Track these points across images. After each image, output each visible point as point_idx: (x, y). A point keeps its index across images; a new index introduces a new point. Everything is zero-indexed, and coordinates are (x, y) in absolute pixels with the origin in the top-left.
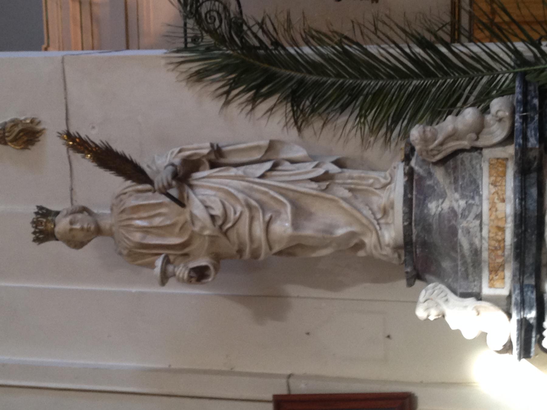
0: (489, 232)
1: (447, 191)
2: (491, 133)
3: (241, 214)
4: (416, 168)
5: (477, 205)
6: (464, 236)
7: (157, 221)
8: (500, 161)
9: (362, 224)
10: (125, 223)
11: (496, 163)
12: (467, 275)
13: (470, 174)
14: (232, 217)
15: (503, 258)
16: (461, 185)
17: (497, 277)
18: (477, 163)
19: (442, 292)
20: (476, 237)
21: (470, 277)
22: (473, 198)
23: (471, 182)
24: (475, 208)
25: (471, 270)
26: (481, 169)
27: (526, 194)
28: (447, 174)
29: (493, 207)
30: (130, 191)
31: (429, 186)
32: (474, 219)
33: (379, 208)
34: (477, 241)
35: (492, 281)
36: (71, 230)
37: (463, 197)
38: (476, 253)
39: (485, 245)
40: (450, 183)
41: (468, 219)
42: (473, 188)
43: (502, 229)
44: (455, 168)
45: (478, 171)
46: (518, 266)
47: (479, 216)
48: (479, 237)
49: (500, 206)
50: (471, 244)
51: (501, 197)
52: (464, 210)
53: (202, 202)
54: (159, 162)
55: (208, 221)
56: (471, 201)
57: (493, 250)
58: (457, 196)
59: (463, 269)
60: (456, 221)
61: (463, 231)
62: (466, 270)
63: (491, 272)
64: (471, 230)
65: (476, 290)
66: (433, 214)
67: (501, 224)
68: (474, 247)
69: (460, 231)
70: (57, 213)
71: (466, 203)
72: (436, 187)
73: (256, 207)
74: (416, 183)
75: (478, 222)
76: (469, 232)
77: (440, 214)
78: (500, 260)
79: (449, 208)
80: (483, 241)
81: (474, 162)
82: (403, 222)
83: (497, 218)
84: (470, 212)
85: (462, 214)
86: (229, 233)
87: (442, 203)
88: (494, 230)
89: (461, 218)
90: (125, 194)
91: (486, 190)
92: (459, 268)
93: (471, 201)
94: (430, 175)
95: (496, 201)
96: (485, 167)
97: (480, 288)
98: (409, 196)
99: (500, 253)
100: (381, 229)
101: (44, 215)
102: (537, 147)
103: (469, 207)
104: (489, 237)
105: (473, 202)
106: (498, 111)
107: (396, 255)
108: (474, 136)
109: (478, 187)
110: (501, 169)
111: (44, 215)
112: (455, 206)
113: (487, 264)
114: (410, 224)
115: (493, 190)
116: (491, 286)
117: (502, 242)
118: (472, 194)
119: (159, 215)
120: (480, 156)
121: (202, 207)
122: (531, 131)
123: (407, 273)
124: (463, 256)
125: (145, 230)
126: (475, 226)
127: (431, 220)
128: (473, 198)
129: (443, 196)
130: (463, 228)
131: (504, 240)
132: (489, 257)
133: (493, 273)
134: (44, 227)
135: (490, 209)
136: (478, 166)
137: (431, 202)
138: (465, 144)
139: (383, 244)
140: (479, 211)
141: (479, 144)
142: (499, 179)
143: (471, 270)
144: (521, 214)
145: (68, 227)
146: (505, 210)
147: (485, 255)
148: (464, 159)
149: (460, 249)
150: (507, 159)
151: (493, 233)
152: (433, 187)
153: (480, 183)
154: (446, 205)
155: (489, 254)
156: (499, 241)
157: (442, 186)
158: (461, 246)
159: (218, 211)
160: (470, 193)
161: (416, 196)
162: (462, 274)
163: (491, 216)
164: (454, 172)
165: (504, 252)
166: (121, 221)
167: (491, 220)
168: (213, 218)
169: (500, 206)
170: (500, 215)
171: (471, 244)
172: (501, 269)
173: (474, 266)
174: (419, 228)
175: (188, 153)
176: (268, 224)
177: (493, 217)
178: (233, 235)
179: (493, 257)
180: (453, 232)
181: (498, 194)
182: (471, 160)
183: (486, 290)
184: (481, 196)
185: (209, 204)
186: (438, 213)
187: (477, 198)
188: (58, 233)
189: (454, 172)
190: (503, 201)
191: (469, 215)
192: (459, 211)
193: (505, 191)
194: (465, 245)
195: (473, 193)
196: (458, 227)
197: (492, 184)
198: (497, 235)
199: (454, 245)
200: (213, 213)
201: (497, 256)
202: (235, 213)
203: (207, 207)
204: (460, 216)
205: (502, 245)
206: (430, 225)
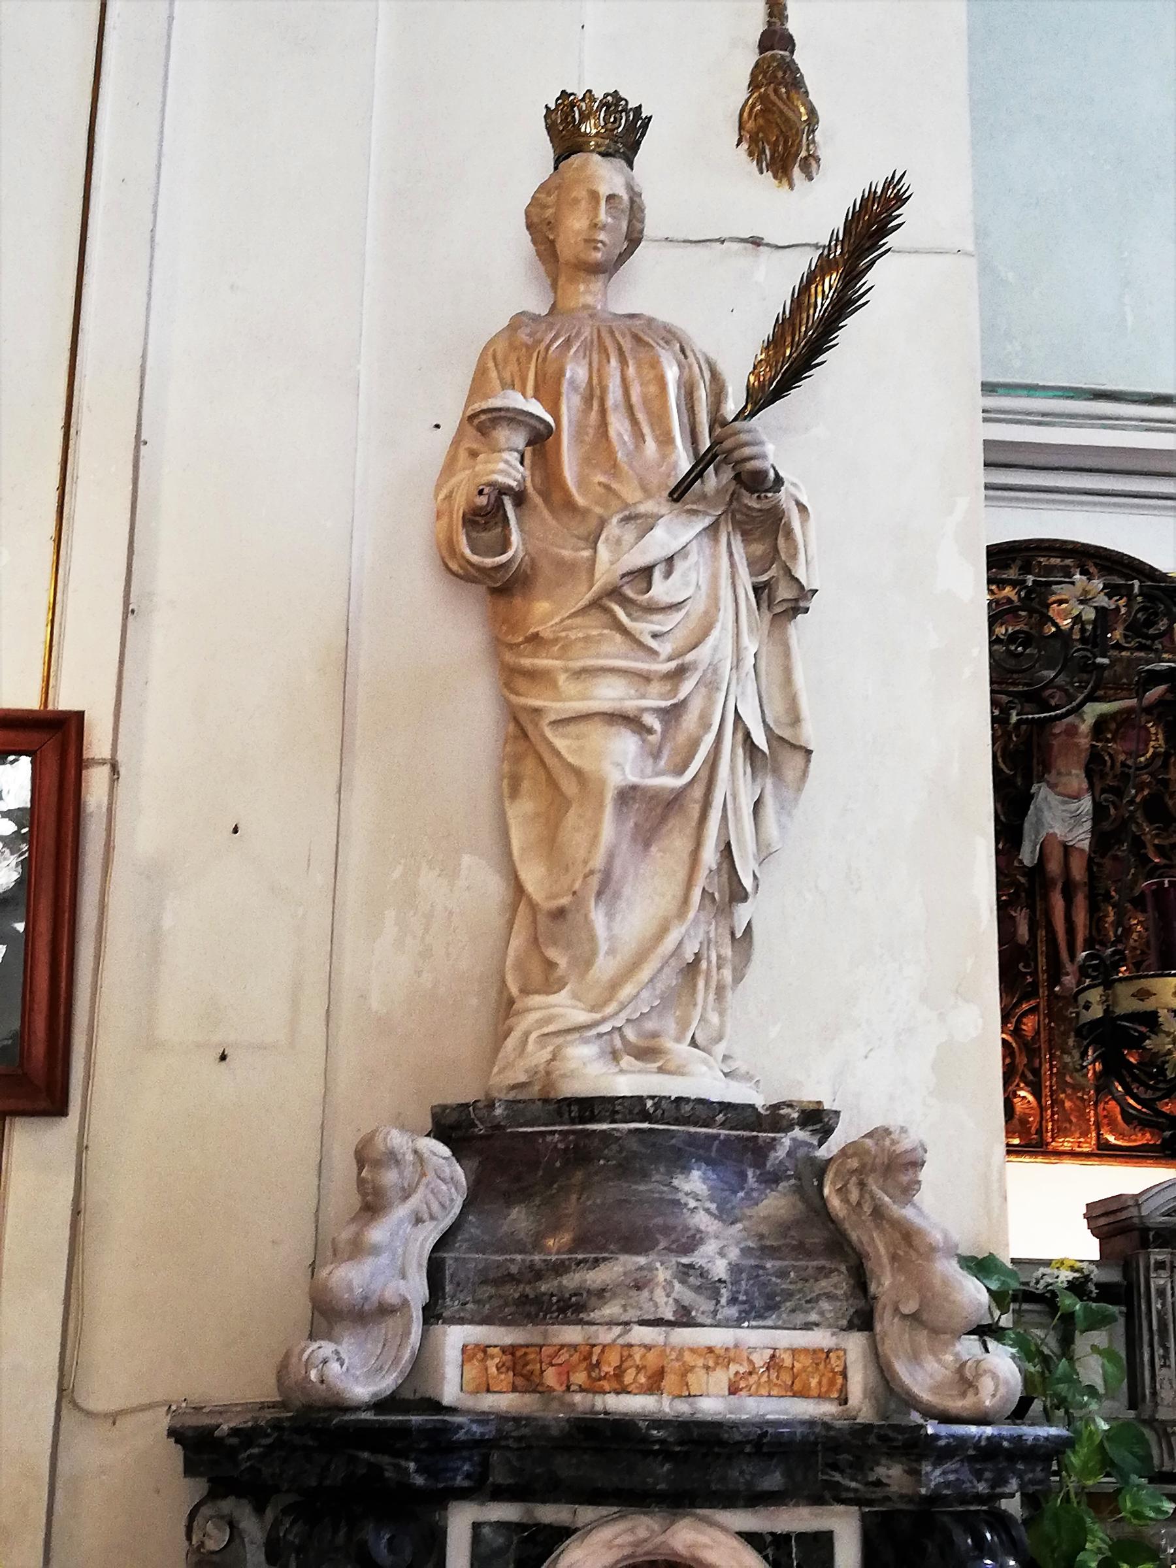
0: (648, 1348)
1: (739, 1226)
2: (915, 1357)
3: (653, 653)
4: (786, 1141)
5: (715, 1312)
6: (625, 1274)
7: (618, 426)
8: (840, 1380)
9: (614, 986)
10: (608, 342)
11: (832, 1370)
12: (498, 1282)
13: (789, 1295)
14: (643, 628)
15: (560, 1389)
16: (763, 1268)
17: (493, 1370)
18: (822, 1313)
19: (443, 1206)
20: (624, 1307)
21: (490, 1290)
22: (733, 1301)
23: (771, 1297)
24: (709, 1306)
25: (513, 1292)
26: (808, 1326)
27: (771, 1455)
28: (784, 1228)
29: (717, 1357)
30: (690, 367)
31: (743, 1176)
32: (676, 1301)
33: (655, 1035)
34: (611, 1310)
35: (480, 1355)
36: (594, 196)
37: (735, 1269)
38: (572, 1308)
39: (606, 1336)
40: (761, 1237)
41: (677, 1285)
42: (759, 1302)
43: (654, 1385)
44: (801, 1250)
45: (800, 1318)
46: (555, 1432)
47: (685, 1318)
48: (625, 1318)
49: (720, 1379)
50: (601, 1294)
51: (742, 1384)
52: (703, 1274)
53: (683, 551)
54: (786, 441)
55: (636, 559)
56: (725, 1294)
57: (589, 1356)
58: (734, 1254)
59: (514, 1269)
60: (668, 1249)
61: (641, 1268)
62: (510, 1278)
63: (509, 1350)
64: (645, 1293)
65: (451, 1306)
66: (676, 1182)
67: (669, 1381)
68: (594, 1301)
69: (642, 1260)
70: (630, 165)
71: (720, 1281)
72: (741, 1194)
73: (675, 691)
74: (748, 1139)
75: (669, 1316)
76: (638, 1288)
77: (677, 1203)
78: (551, 1377)
79: (699, 1231)
80: (617, 1330)
81: (825, 1305)
82: (652, 1098)
83: (687, 1370)
84: (698, 1289)
85: (691, 1266)
86: (596, 617)
87: (707, 1210)
88: (652, 1358)
89: (678, 1263)
90: (683, 351)
91: (759, 1339)
92: (519, 1257)
93: (725, 1294)
94: (772, 1179)
95: (733, 1368)
96: (820, 1338)
97: (461, 1321)
98: (720, 1117)
99: (580, 1377)
100: (600, 1035)
101: (626, 131)
102: (923, 1491)
103: (711, 1288)
104: (630, 1346)
105: (723, 1301)
106: (995, 1376)
107: (523, 1078)
108: (909, 1308)
109: (760, 1316)
110: (814, 1382)
111: (626, 131)
112: (710, 1248)
113: (538, 1340)
114: (645, 1116)
115: (761, 1359)
116: (469, 1353)
117: (616, 1386)
118: (742, 1298)
119: (639, 436)
120: (844, 1322)
121: (675, 546)
122: (955, 1471)
123: (491, 1105)
124: (560, 1269)
125: (594, 395)
126: (656, 1306)
127: (657, 1177)
128: (733, 1301)
129: (726, 1215)
130: (650, 1268)
131: (623, 1390)
132: (562, 1346)
133: (507, 1358)
134: (594, 129)
135: (710, 1350)
136: (814, 1317)
137: (705, 1180)
138: (885, 1283)
139: (560, 1040)
140: (701, 1319)
141: (885, 1323)
142: (787, 1378)
143: (513, 1292)
144: (721, 1443)
145: (604, 191)
146: (708, 1396)
147: (572, 1334)
148: (835, 1278)
149: (585, 1261)
150: (844, 1401)
151: (643, 1357)
152: (742, 1189)
153: (769, 1323)
154: (702, 1220)
155: (574, 1347)
156: (619, 1373)
157: (748, 1212)
158: (596, 1262)
159: (661, 590)
160: (746, 1293)
161: (716, 1137)
162: (499, 1265)
163: (692, 1350)
164: (794, 1248)
165: (582, 1390)
166: (612, 333)
167: (681, 1351)
168: (646, 573)
169: (720, 1379)
170: (696, 1380)
171: (601, 1294)
172: (520, 1381)
173: (524, 1300)
174: (633, 1144)
175: (796, 525)
176: (631, 721)
177: (688, 1357)
178: (593, 626)
179: (564, 1356)
180: (635, 1242)
181: (750, 1373)
182: (830, 1297)
183: (455, 1338)
184: (737, 1323)
185: (680, 566)
186: (680, 1196)
187: (733, 1312)
188: (583, 167)
189: (794, 1248)
190: (733, 1390)
191: (691, 1287)
192: (696, 1259)
193: (756, 1394)
194: (595, 1278)
195: (744, 1303)
196: (652, 1256)
197: (773, 1357)
198: (639, 1369)
199: (596, 1243)
200: (657, 574)
201: (566, 1371)
202: (655, 636)
203: (670, 560)
204: (685, 1260)
205: (606, 1385)
206: (645, 1175)
